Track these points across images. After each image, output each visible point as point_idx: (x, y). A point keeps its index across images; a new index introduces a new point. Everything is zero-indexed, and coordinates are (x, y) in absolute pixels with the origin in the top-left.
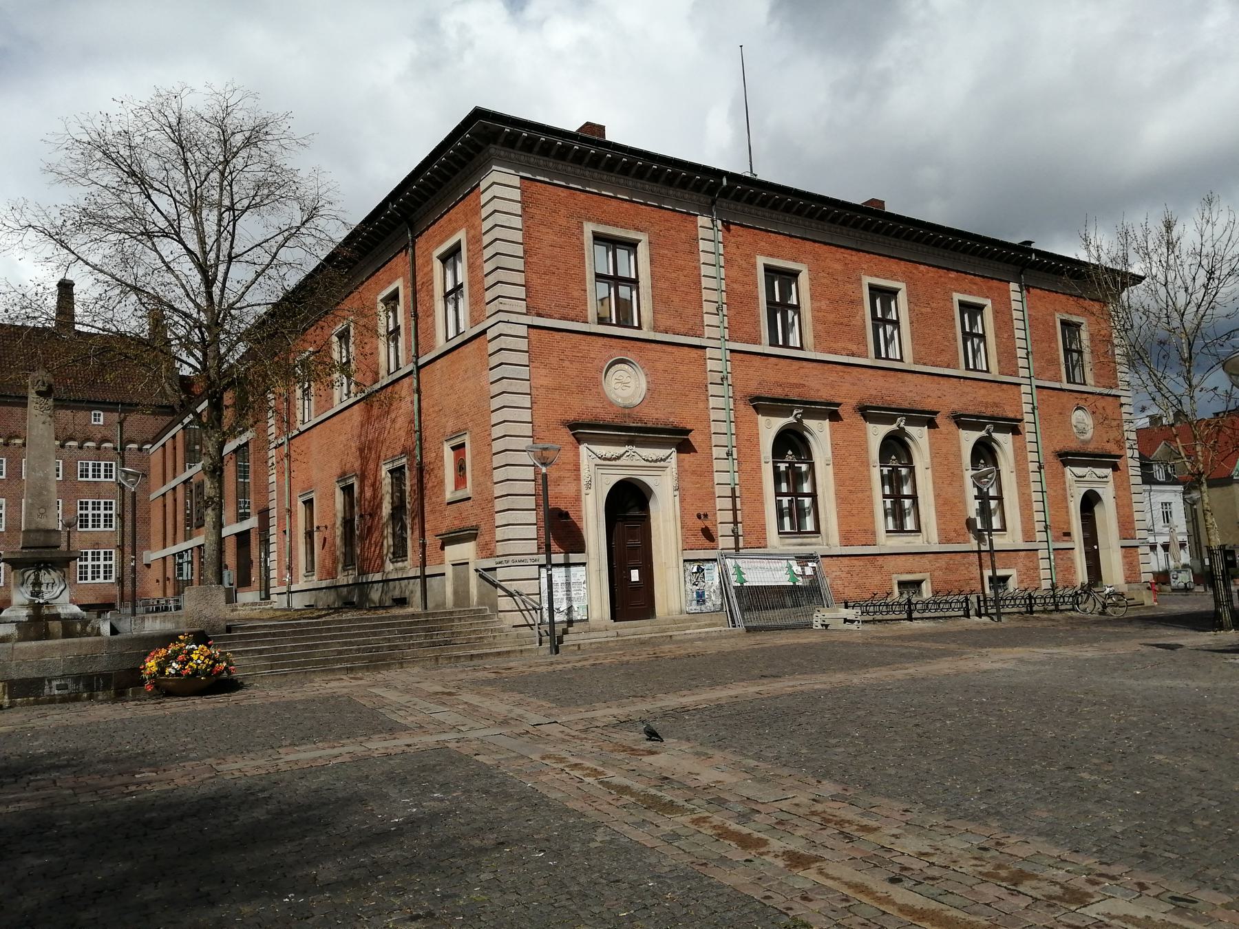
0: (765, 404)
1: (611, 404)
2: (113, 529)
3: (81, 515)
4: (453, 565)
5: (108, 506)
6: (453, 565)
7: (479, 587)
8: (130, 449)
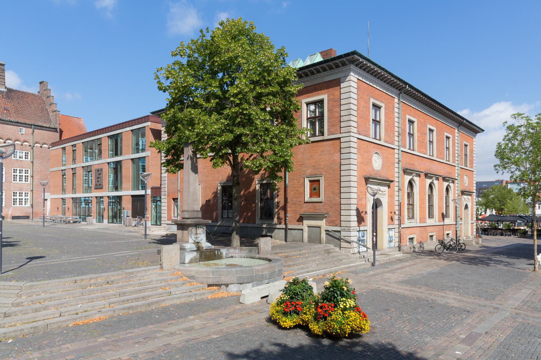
0: (406, 171)
1: (374, 170)
2: (29, 182)
3: (14, 175)
4: (308, 227)
5: (26, 172)
6: (308, 227)
7: (326, 238)
8: (37, 146)
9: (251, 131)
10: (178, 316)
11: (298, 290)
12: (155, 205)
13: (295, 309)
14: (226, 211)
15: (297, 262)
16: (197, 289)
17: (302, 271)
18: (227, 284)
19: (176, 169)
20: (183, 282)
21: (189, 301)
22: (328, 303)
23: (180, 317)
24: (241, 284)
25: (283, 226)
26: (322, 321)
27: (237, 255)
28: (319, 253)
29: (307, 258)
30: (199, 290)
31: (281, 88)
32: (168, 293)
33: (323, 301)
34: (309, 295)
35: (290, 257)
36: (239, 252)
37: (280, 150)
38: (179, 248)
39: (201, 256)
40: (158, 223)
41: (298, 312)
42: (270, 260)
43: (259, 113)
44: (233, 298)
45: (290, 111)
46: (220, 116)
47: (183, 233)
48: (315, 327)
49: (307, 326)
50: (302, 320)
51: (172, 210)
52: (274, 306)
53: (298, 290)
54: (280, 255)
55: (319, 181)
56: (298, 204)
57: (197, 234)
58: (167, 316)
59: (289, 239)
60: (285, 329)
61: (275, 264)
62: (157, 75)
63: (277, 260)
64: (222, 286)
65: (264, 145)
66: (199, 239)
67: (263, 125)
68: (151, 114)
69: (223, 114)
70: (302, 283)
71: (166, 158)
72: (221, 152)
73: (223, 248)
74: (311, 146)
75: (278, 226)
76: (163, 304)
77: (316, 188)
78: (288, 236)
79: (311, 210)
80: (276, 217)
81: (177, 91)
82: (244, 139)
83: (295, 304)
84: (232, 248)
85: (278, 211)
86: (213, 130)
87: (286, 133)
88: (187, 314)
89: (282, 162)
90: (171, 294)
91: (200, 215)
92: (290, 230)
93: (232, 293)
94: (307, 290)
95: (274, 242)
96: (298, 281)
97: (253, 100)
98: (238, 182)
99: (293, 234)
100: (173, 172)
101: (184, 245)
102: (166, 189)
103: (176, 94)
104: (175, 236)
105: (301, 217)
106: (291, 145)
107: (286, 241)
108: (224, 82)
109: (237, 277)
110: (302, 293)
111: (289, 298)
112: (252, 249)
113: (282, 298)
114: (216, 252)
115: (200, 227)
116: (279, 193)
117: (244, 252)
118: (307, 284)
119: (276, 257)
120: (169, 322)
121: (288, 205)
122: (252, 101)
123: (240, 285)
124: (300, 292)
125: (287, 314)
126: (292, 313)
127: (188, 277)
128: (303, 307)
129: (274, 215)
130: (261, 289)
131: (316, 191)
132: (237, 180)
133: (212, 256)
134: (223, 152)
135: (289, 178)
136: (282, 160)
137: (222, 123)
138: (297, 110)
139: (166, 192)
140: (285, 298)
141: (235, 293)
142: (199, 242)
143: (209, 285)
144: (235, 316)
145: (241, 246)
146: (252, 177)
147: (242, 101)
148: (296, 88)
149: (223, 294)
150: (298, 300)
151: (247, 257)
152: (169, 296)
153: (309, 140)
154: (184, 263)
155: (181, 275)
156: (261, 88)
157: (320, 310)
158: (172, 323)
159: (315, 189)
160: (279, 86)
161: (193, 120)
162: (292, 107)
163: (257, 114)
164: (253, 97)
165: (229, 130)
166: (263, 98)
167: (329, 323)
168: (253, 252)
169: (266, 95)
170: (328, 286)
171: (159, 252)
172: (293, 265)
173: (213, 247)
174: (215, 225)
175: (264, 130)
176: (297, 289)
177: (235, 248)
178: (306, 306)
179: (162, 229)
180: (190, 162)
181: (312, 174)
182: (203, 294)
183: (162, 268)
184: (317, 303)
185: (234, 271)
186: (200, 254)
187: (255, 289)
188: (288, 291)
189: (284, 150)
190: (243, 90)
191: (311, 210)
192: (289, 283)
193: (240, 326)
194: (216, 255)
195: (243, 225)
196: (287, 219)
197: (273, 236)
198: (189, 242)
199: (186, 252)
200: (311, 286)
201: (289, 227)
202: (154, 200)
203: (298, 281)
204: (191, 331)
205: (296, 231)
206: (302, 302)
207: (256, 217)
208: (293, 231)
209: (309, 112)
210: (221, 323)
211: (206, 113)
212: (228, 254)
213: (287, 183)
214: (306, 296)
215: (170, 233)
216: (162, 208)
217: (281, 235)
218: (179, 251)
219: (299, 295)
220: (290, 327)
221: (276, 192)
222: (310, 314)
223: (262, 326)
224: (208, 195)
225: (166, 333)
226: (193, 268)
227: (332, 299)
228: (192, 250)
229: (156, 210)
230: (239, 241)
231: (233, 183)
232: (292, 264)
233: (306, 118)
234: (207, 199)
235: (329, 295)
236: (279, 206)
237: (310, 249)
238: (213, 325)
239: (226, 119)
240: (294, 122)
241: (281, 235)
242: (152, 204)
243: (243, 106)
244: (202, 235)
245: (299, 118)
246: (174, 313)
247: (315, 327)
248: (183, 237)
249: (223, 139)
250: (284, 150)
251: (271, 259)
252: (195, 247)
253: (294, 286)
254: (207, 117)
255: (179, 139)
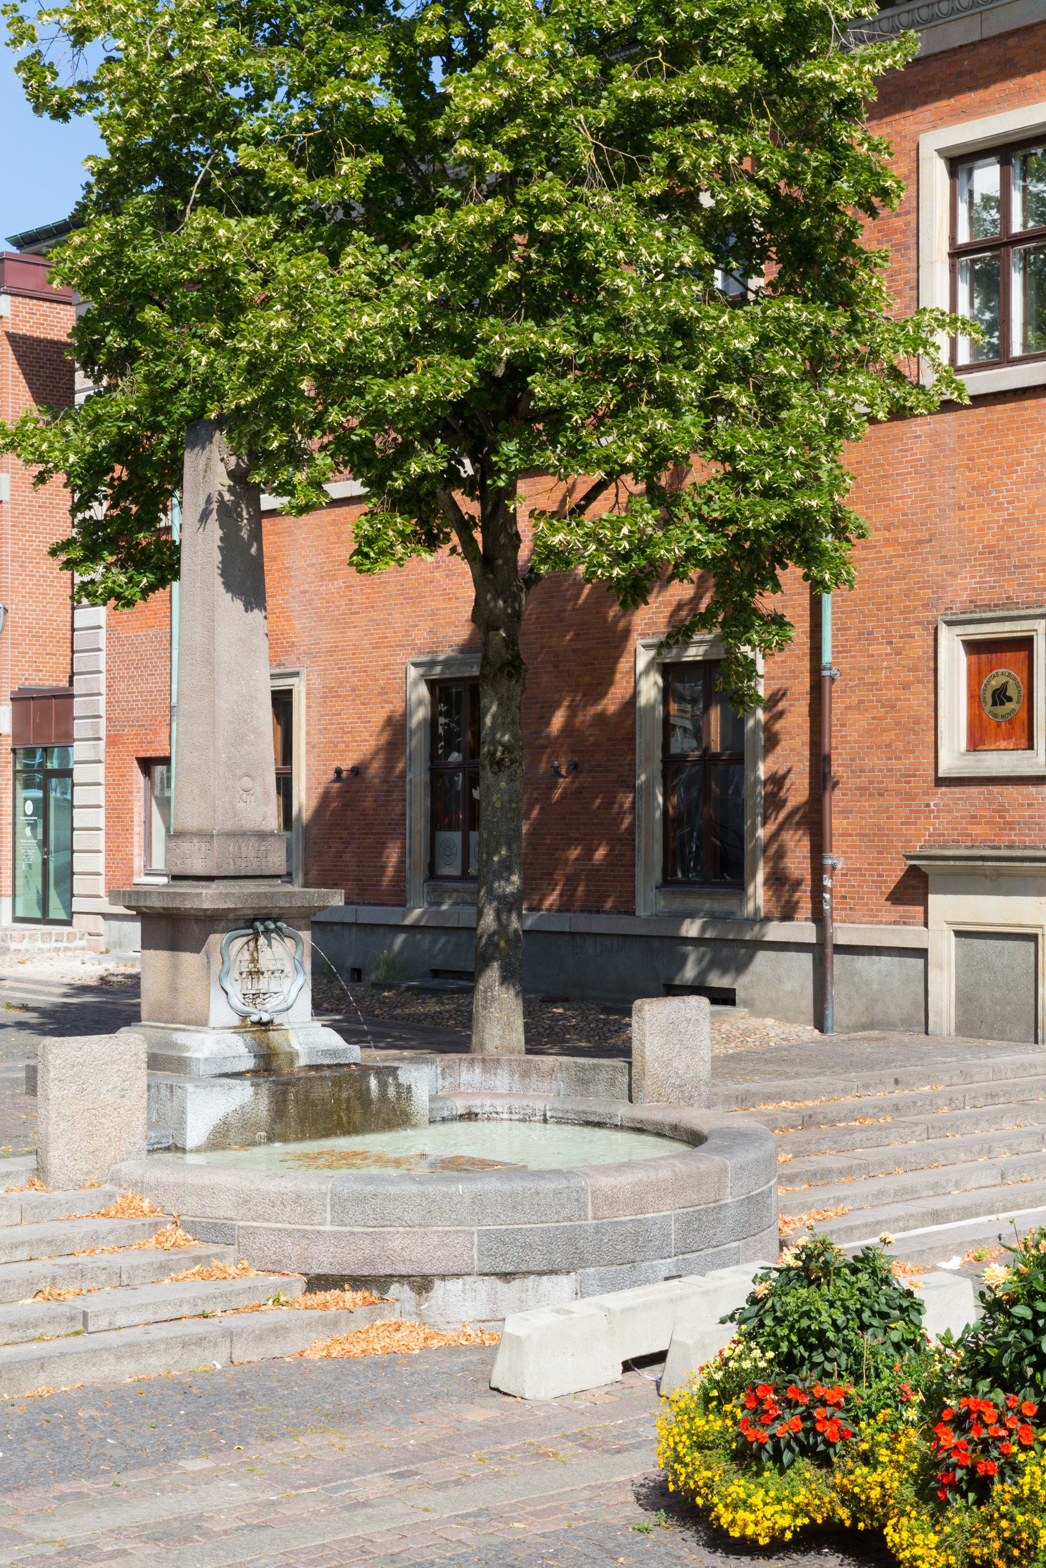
4: (958, 934)
6: (958, 934)
9: (586, 340)
10: (119, 1453)
11: (824, 1317)
12: (34, 801)
13: (807, 1431)
14: (457, 836)
15: (872, 1155)
16: (243, 1301)
17: (900, 1209)
18: (424, 1277)
19: (137, 578)
20: (162, 1257)
21: (192, 1373)
22: (999, 1396)
23: (135, 1461)
24: (506, 1276)
25: (803, 931)
26: (960, 1502)
27: (501, 1105)
28: (1023, 1102)
29: (934, 1129)
30: (256, 1308)
31: (774, 65)
32: (72, 1319)
33: (974, 1385)
34: (897, 1347)
35: (832, 1123)
36: (517, 1087)
37: (762, 452)
38: (144, 1057)
39: (279, 1112)
40: (56, 911)
41: (821, 1448)
42: (695, 1139)
43: (630, 226)
44: (454, 1359)
45: (833, 207)
46: (398, 253)
47: (175, 967)
48: (919, 1538)
49: (876, 1535)
50: (849, 1498)
51: (138, 829)
52: (686, 1411)
53: (824, 1317)
54: (771, 1107)
55: (1025, 644)
56: (898, 793)
57: (256, 973)
58: (57, 1450)
59: (837, 1011)
60: (745, 1547)
61: (718, 1159)
62: (21, 19)
63: (738, 1138)
64: (395, 1290)
65: (662, 424)
66: (272, 1003)
67: (657, 302)
68: (14, 250)
69: (418, 238)
70: (855, 1271)
71: (80, 516)
72: (398, 469)
73: (411, 1060)
74: (977, 426)
75: (776, 931)
76: (40, 1385)
77: (1011, 692)
78: (836, 991)
79: (976, 830)
80: (760, 877)
81: (134, 112)
82: (538, 384)
83: (806, 1400)
84: (472, 1062)
85: (774, 836)
86: (350, 342)
87: (803, 345)
88: (171, 1443)
89: (775, 527)
90: (85, 1324)
91: (276, 860)
92: (847, 957)
93: (450, 1333)
94: (884, 1316)
95: (746, 1033)
96: (826, 1263)
97: (598, 150)
98: (517, 657)
99: (868, 983)
100: (119, 597)
101: (180, 1038)
102: (102, 700)
103: (134, 126)
104: (132, 985)
105: (913, 872)
106: (837, 425)
107: (820, 1024)
108: (416, 46)
109: (483, 1234)
110: (852, 1336)
111: (770, 1362)
112: (595, 1067)
113: (731, 1364)
114: (373, 1083)
115: (279, 931)
116: (778, 726)
117: (546, 1085)
118: (886, 1281)
119: (739, 1120)
120: (65, 1488)
121: (836, 800)
122: (587, 157)
123: (499, 1284)
124: (837, 1329)
125: (758, 1459)
126: (787, 1457)
127: (191, 1228)
128: (856, 1420)
129: (747, 869)
130: (622, 1311)
131: (1009, 706)
132: (511, 642)
133: (348, 1109)
134: (415, 468)
135: (839, 629)
136: (778, 511)
137: (406, 298)
138: (876, 201)
139: (103, 722)
140: (747, 1365)
141: (469, 1331)
142: (270, 1022)
143: (317, 1283)
144: (454, 1468)
145: (528, 1052)
146: (616, 623)
147: (531, 163)
148: (863, 62)
149: (398, 1336)
150: (828, 1374)
151: (559, 1121)
152: (79, 1339)
153: (960, 389)
154: (178, 1148)
155: (152, 1218)
156: (643, 74)
157: (950, 1438)
158: (79, 1495)
159: (1000, 696)
160: (759, 56)
161: (228, 283)
162: (843, 185)
163: (623, 238)
164: (595, 132)
165: (449, 334)
166: (658, 137)
167: (1003, 1516)
168: (601, 1087)
169: (681, 119)
170: (999, 1294)
171: (32, 1082)
172: (847, 1172)
173: (356, 1053)
174: (392, 922)
175: (661, 329)
176: (823, 1306)
177: (490, 1064)
178: (872, 1415)
179: (78, 943)
180: (214, 531)
181: (985, 598)
182: (278, 1331)
183: (40, 1171)
184: (933, 1401)
185: (467, 1200)
186: (273, 1094)
187: (587, 1307)
188: (769, 1321)
189: (791, 450)
190: (534, 93)
191: (976, 830)
192: (775, 1275)
193: (475, 1524)
194: (370, 1101)
195: (561, 923)
196: (827, 883)
197: (740, 995)
198: (212, 1022)
199: (192, 1080)
200: (909, 1294)
201: (841, 939)
202: (28, 769)
203: (826, 1263)
204: (187, 1540)
205: (884, 962)
206: (852, 1391)
207: (639, 871)
208: (861, 962)
209: (963, 209)
210: (365, 1504)
211: (314, 238)
212: (442, 1098)
213: (827, 657)
214: (874, 1354)
215: (122, 970)
216: (80, 818)
217: (788, 987)
218: (142, 1077)
219: (833, 1345)
220: (772, 1537)
221: (761, 715)
222: (898, 1466)
223: (608, 1527)
224: (348, 738)
225: (43, 1549)
226: (225, 1179)
227: (1022, 1374)
228: (228, 1069)
229: (40, 830)
230: (519, 1023)
231: (485, 662)
232: (836, 1165)
233: (945, 248)
234: (346, 765)
235: (1008, 1345)
236: (783, 803)
237: (966, 1075)
238: (317, 1513)
239: (429, 271)
240: (863, 274)
241: (788, 987)
242: (22, 794)
243: (534, 189)
244: (286, 983)
245: (900, 248)
246: (95, 1435)
247: (919, 1538)
248: (174, 989)
249: (413, 390)
250: (791, 450)
251: (704, 1128)
252: (243, 1050)
253: (803, 1292)
254: (318, 258)
255: (152, 396)
